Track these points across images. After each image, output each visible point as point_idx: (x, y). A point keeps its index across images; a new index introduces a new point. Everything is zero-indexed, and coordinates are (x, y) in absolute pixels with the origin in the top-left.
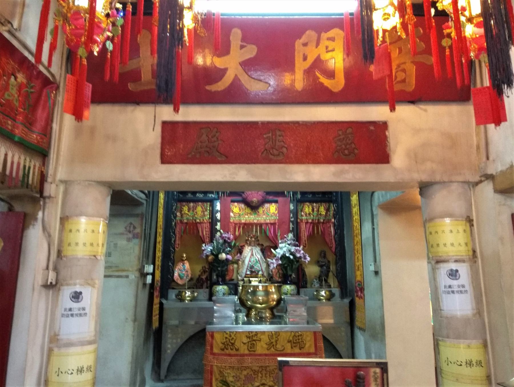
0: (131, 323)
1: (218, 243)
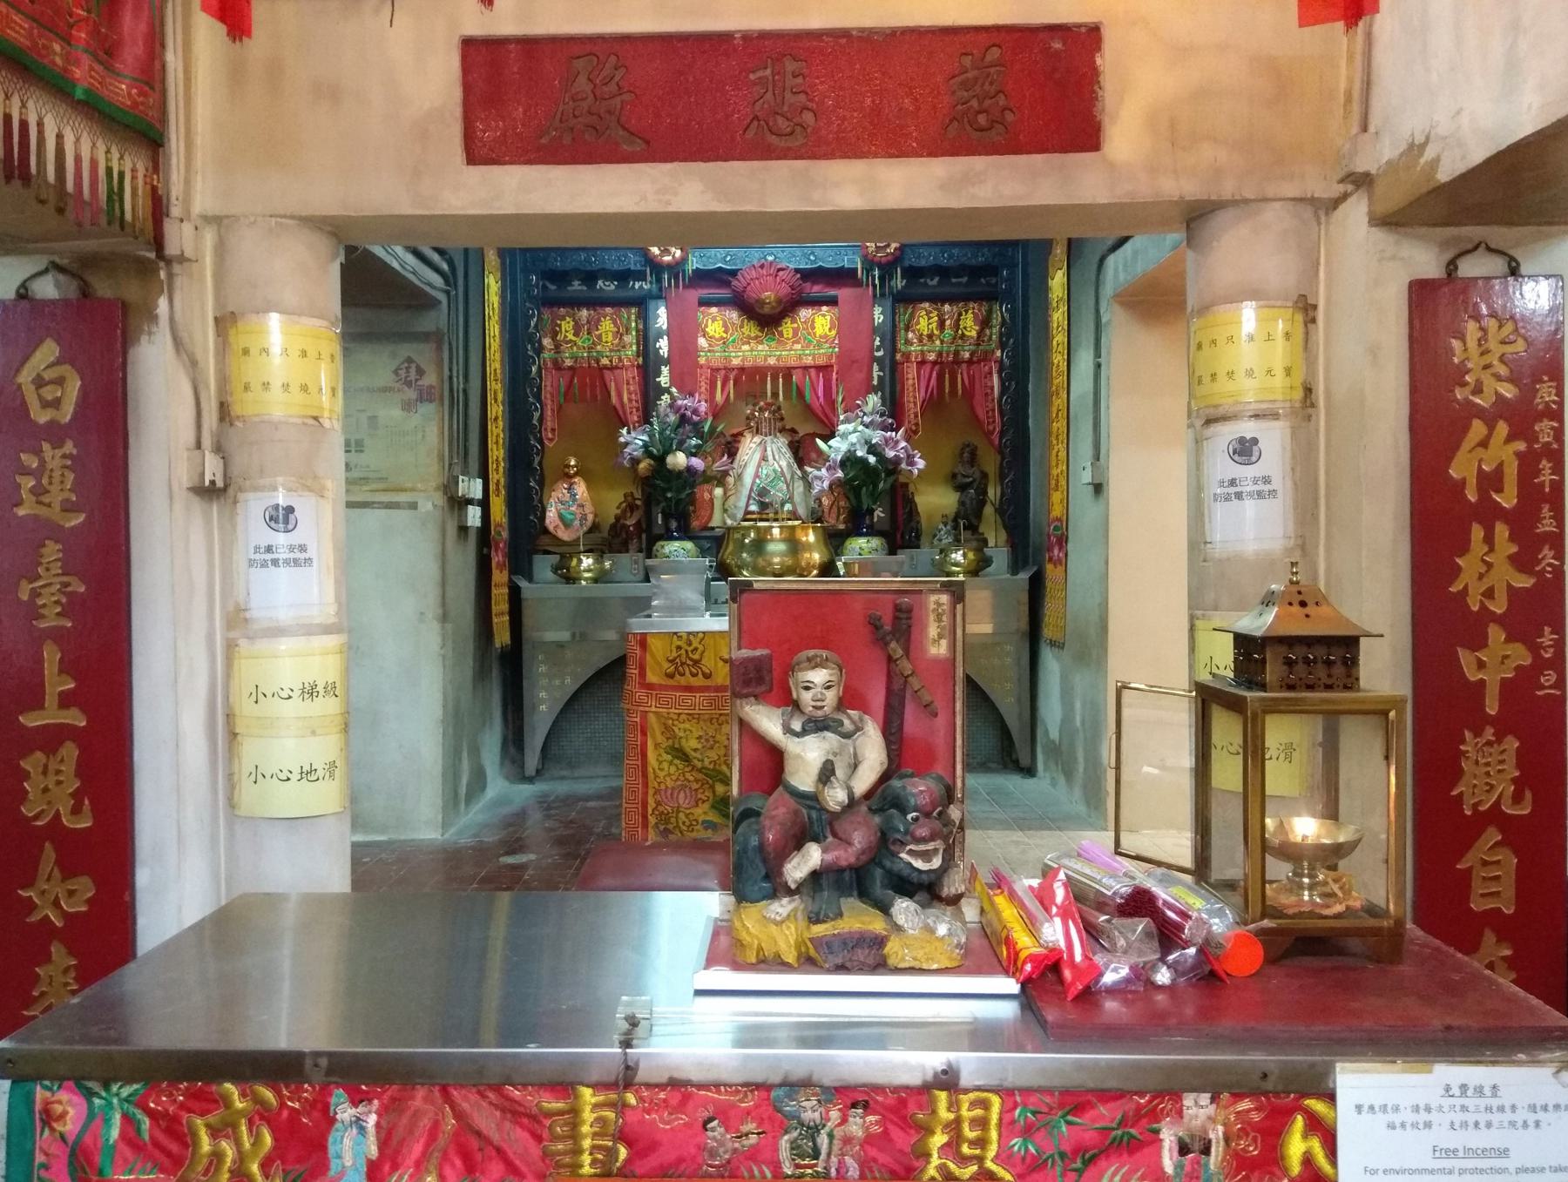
0: (436, 626)
1: (663, 423)
